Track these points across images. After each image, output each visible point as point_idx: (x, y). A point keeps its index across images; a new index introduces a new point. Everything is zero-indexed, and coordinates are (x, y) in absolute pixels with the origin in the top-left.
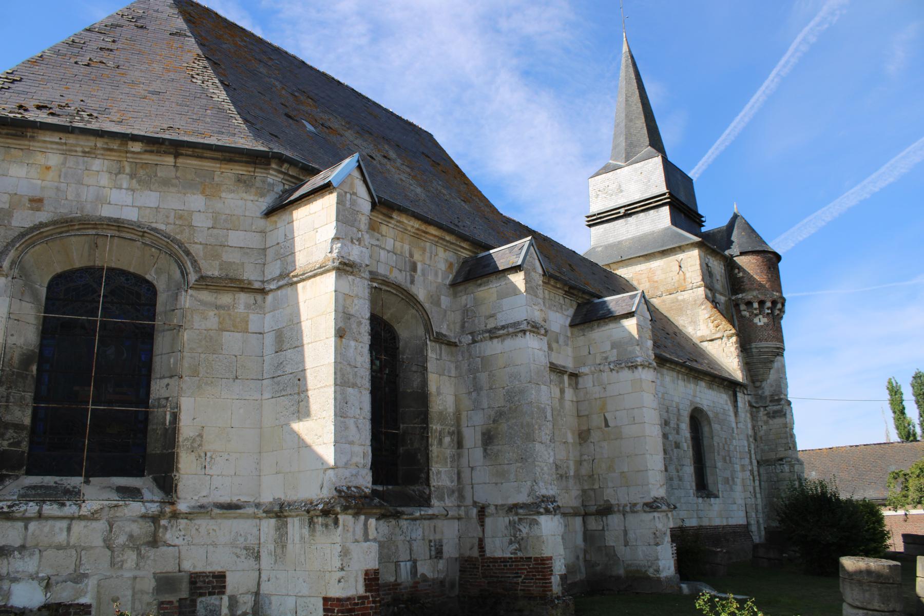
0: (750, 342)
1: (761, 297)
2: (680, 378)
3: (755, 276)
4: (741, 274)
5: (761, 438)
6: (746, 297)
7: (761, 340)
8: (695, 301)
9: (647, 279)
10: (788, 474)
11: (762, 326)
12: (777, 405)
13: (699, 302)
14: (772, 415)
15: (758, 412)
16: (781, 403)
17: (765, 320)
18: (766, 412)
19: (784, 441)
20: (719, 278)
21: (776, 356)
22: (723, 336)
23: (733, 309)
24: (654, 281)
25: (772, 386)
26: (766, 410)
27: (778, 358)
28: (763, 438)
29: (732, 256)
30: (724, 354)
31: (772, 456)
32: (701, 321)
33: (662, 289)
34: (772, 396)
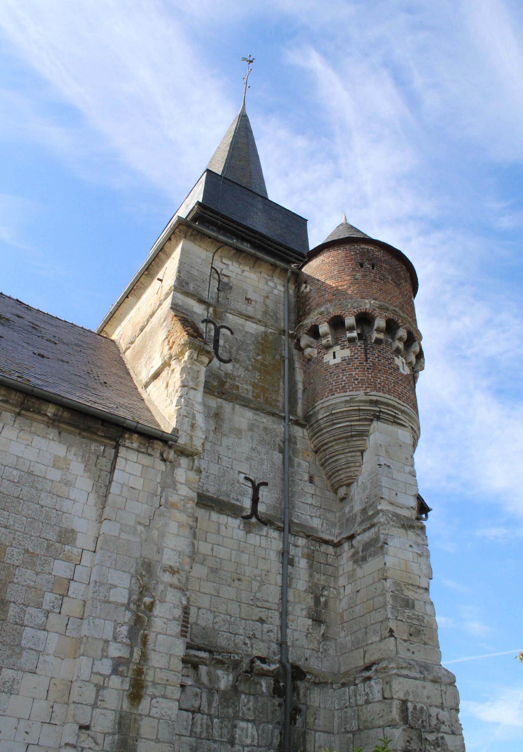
1: (334, 311)
3: (328, 282)
7: (332, 392)
10: (377, 707)
11: (337, 366)
12: (370, 528)
15: (337, 556)
17: (347, 353)
18: (353, 550)
19: (378, 616)
21: (372, 420)
34: (364, 511)
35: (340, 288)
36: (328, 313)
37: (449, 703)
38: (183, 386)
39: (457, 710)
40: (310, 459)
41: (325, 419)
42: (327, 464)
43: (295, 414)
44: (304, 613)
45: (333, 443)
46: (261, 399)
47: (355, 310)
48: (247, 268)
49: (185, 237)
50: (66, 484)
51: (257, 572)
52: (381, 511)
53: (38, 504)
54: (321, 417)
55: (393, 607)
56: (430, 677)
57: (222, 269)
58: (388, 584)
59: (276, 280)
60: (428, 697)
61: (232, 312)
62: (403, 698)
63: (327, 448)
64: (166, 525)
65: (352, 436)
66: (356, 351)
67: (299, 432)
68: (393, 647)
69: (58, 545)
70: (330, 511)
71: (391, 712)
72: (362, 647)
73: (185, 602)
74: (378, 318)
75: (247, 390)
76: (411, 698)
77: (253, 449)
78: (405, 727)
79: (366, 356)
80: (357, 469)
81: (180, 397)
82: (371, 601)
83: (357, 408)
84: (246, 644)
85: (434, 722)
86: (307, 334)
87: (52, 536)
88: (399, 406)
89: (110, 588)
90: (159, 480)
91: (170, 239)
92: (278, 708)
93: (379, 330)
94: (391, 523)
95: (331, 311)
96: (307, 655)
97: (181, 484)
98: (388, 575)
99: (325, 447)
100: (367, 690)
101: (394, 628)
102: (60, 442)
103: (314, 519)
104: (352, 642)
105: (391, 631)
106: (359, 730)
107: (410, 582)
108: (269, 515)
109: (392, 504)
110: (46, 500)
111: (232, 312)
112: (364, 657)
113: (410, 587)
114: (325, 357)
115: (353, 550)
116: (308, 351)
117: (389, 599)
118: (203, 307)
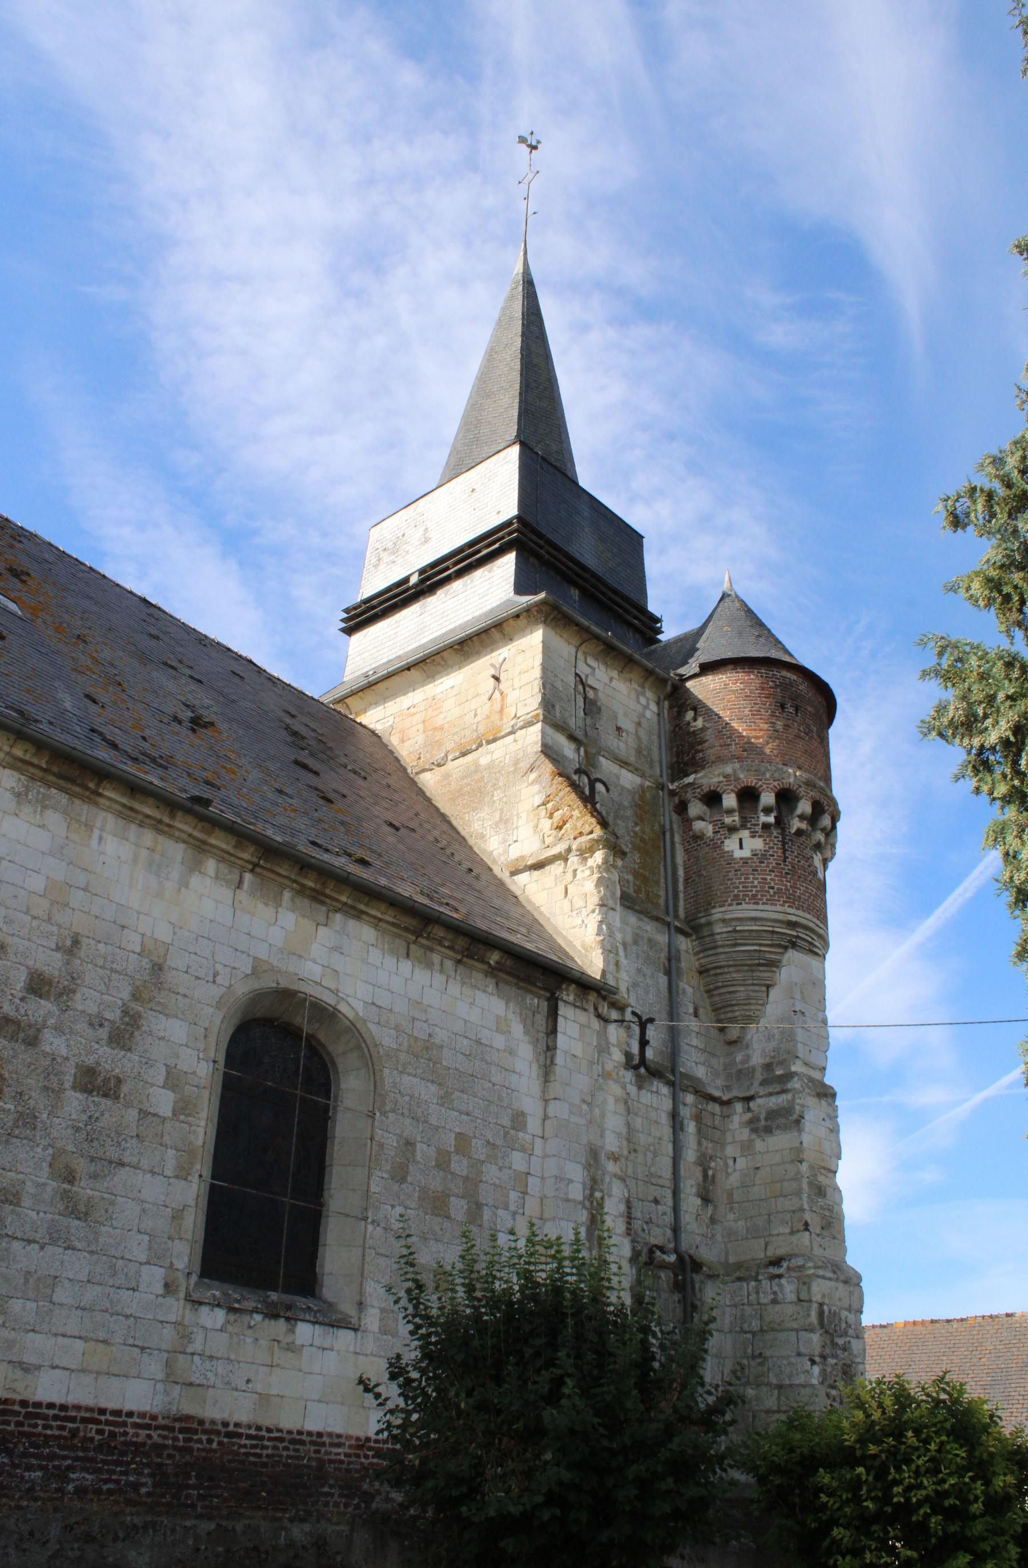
0: (709, 906)
1: (747, 779)
2: (246, 885)
3: (734, 725)
4: (700, 723)
5: (730, 1194)
6: (704, 781)
7: (738, 900)
8: (516, 763)
9: (421, 726)
10: (790, 1309)
11: (745, 861)
12: (778, 1093)
13: (524, 765)
14: (763, 1123)
16: (789, 1086)
17: (758, 844)
18: (749, 1115)
19: (788, 1204)
20: (627, 725)
21: (786, 948)
22: (569, 850)
23: (675, 816)
24: (435, 729)
25: (770, 1038)
26: (749, 1109)
27: (794, 960)
28: (736, 1197)
29: (683, 679)
30: (566, 903)
31: (756, 1251)
32: (524, 815)
33: (449, 745)
34: (768, 1067)
35: (753, 740)
36: (737, 779)
37: (855, 1306)
38: (602, 905)
39: (861, 1312)
40: (694, 982)
41: (724, 935)
42: (716, 992)
43: (676, 916)
44: (694, 1190)
45: (731, 969)
46: (642, 896)
47: (776, 783)
48: (615, 674)
49: (545, 622)
50: (510, 1053)
51: (650, 1140)
52: (796, 1073)
53: (490, 1081)
54: (719, 931)
55: (809, 1197)
56: (842, 1278)
57: (587, 676)
58: (804, 1168)
59: (649, 694)
60: (840, 1300)
61: (606, 754)
62: (820, 1300)
63: (722, 974)
64: (605, 1101)
65: (759, 965)
66: (772, 844)
67: (684, 944)
68: (807, 1243)
69: (512, 1132)
70: (714, 1055)
71: (809, 1315)
72: (764, 1237)
73: (626, 1195)
74: (803, 800)
75: (628, 881)
76: (827, 1301)
77: (639, 971)
78: (821, 1331)
79: (784, 853)
80: (759, 1007)
81: (601, 922)
82: (779, 1185)
83: (771, 929)
84: (643, 1230)
85: (843, 1325)
86: (700, 800)
87: (506, 1121)
88: (817, 929)
89: (568, 1184)
90: (595, 1044)
91: (518, 616)
92: (678, 1305)
93: (802, 817)
94: (807, 1090)
95: (742, 776)
96: (698, 1242)
97: (614, 1046)
98: (805, 1157)
99: (718, 971)
100: (776, 1288)
101: (809, 1221)
102: (499, 996)
103: (700, 1066)
104: (748, 1230)
105: (806, 1224)
106: (762, 1330)
107: (823, 1164)
108: (657, 1063)
109: (806, 1064)
110: (497, 1077)
111: (606, 754)
112: (766, 1249)
113: (822, 1171)
114: (727, 842)
115: (749, 1115)
116: (698, 826)
117: (805, 1186)
118: (573, 746)
